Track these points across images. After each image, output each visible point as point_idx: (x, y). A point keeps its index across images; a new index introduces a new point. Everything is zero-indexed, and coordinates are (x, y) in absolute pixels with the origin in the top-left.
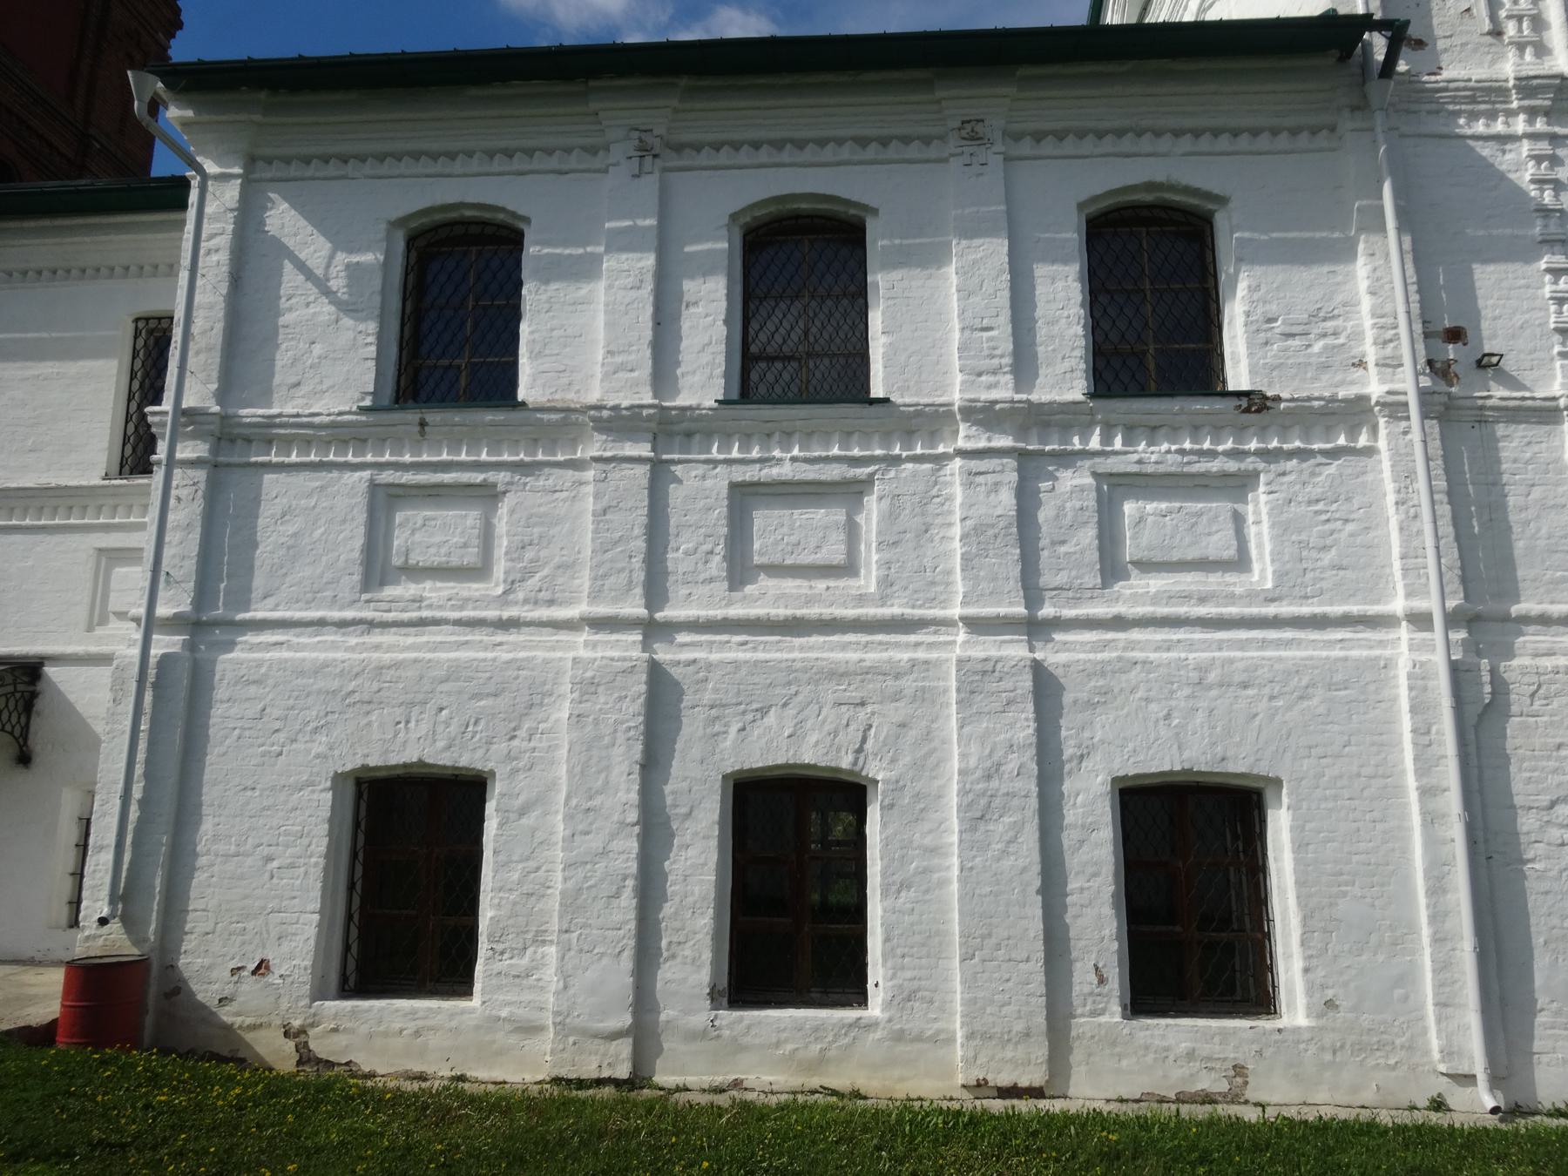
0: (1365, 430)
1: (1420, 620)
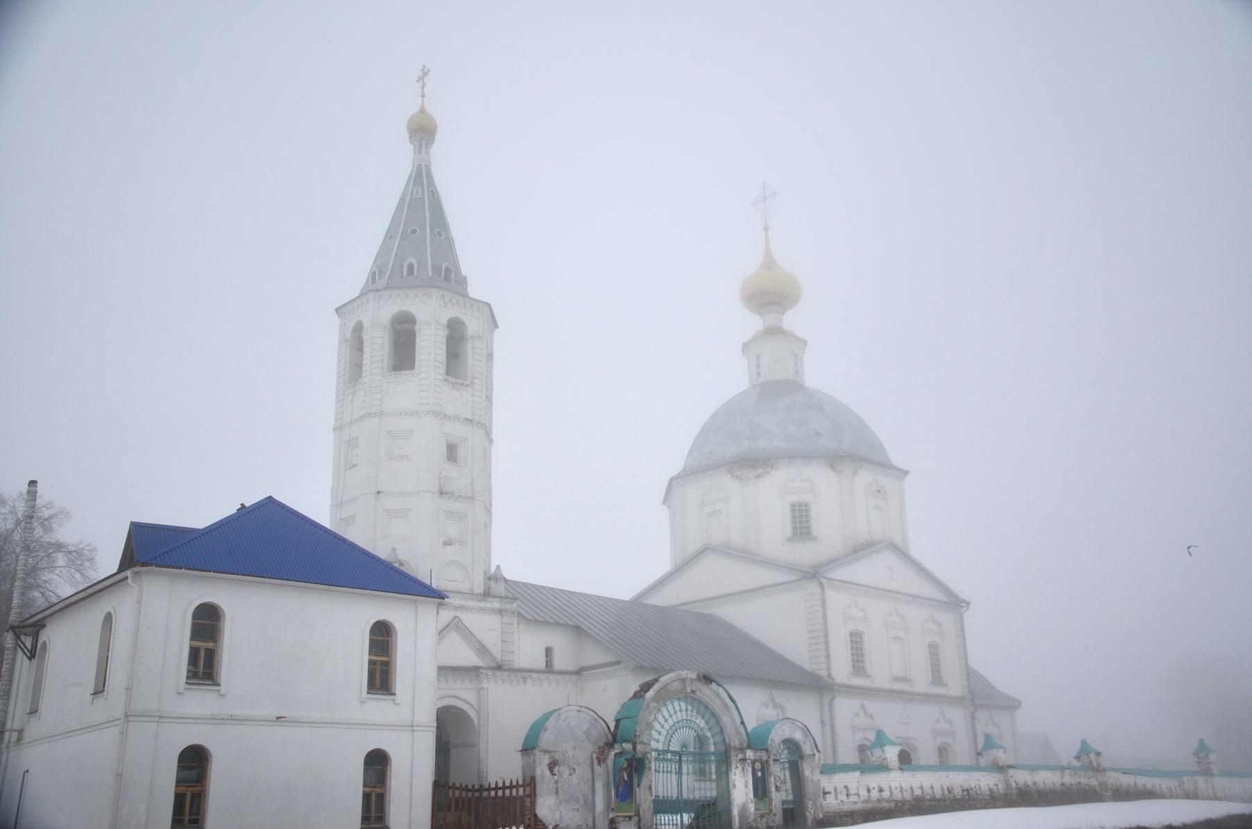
0: (492, 572)
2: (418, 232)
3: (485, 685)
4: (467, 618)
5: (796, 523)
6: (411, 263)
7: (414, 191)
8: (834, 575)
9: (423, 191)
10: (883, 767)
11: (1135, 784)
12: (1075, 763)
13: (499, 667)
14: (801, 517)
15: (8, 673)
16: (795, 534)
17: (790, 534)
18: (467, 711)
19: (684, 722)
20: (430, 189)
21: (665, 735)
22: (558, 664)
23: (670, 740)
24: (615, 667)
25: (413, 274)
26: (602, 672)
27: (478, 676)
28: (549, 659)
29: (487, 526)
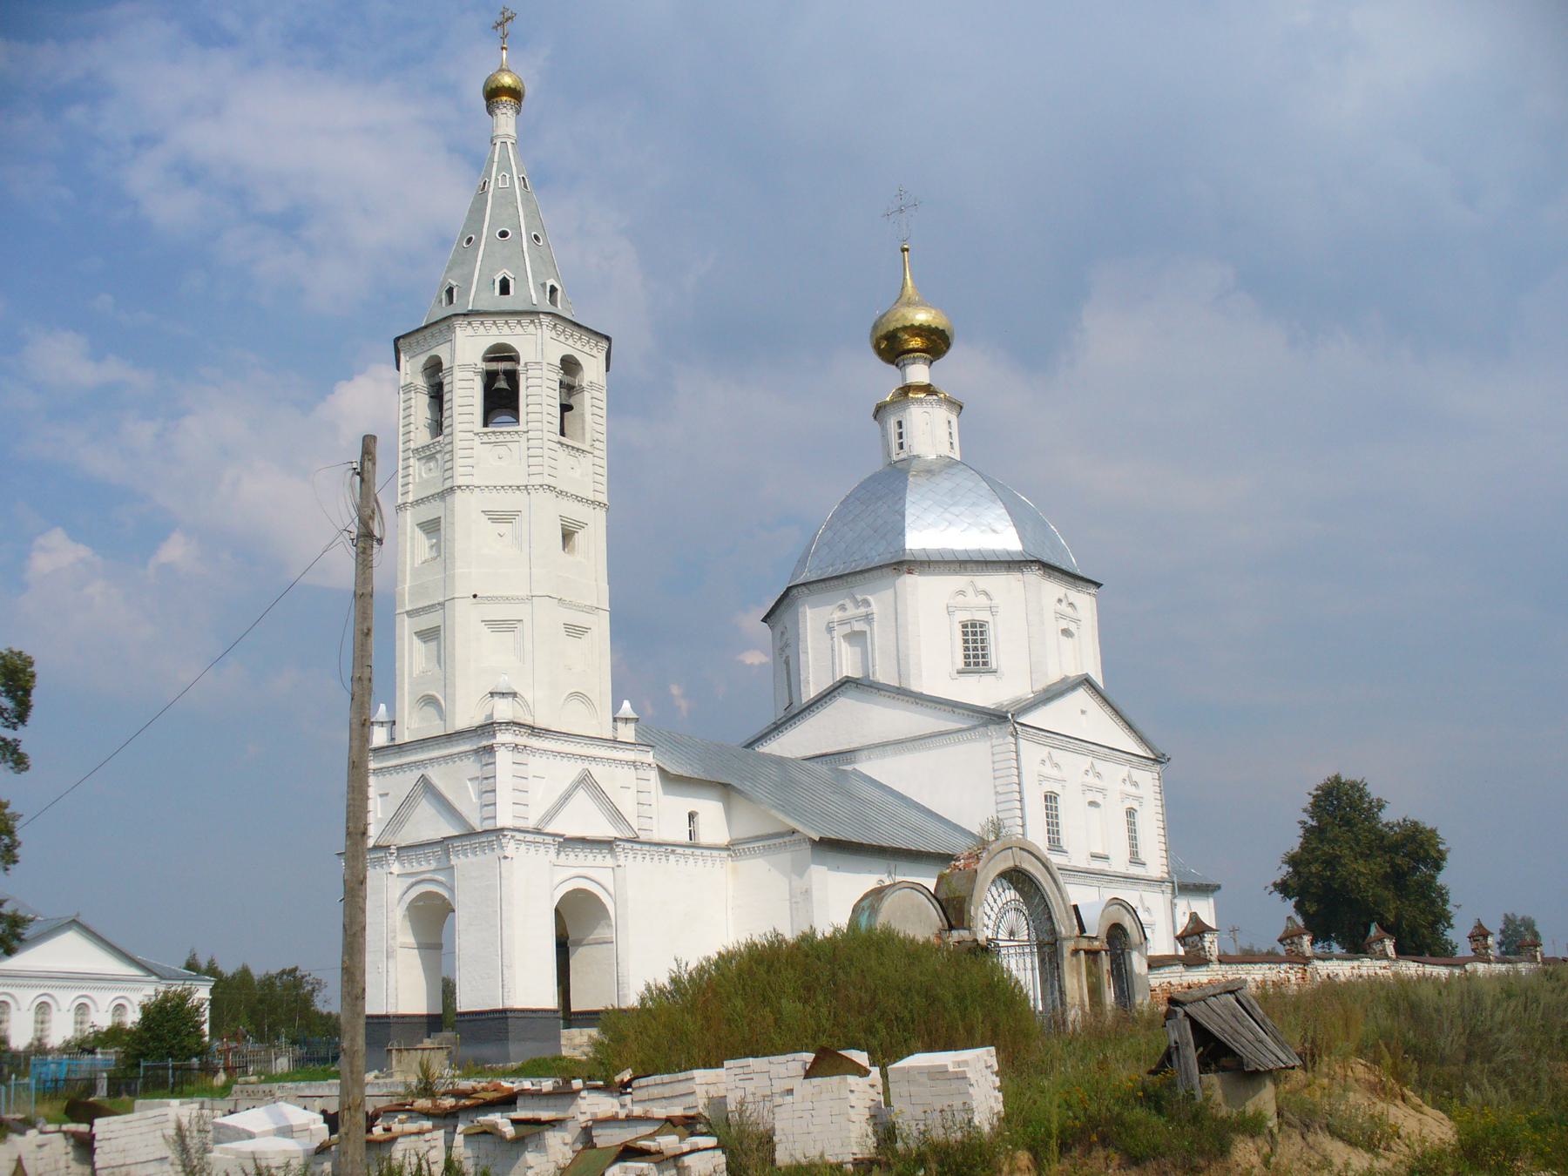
1: (202, 1107)
2: (510, 235)
3: (622, 861)
4: (597, 771)
5: (969, 658)
6: (505, 278)
7: (499, 178)
8: (1022, 720)
9: (512, 178)
10: (1205, 962)
11: (1424, 973)
12: (1281, 950)
13: (634, 841)
14: (975, 649)
15: (297, 1047)
16: (967, 664)
17: (960, 664)
18: (601, 897)
19: (1013, 902)
20: (521, 176)
21: (994, 919)
22: (705, 837)
23: (999, 927)
24: (787, 839)
25: (509, 293)
26: (764, 846)
27: (612, 850)
28: (692, 828)
29: (348, 820)
